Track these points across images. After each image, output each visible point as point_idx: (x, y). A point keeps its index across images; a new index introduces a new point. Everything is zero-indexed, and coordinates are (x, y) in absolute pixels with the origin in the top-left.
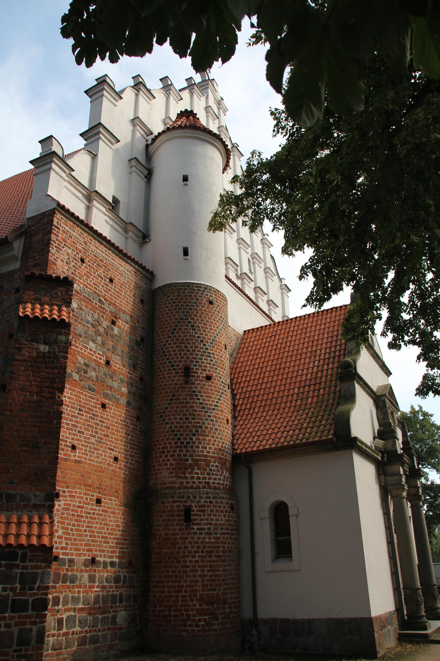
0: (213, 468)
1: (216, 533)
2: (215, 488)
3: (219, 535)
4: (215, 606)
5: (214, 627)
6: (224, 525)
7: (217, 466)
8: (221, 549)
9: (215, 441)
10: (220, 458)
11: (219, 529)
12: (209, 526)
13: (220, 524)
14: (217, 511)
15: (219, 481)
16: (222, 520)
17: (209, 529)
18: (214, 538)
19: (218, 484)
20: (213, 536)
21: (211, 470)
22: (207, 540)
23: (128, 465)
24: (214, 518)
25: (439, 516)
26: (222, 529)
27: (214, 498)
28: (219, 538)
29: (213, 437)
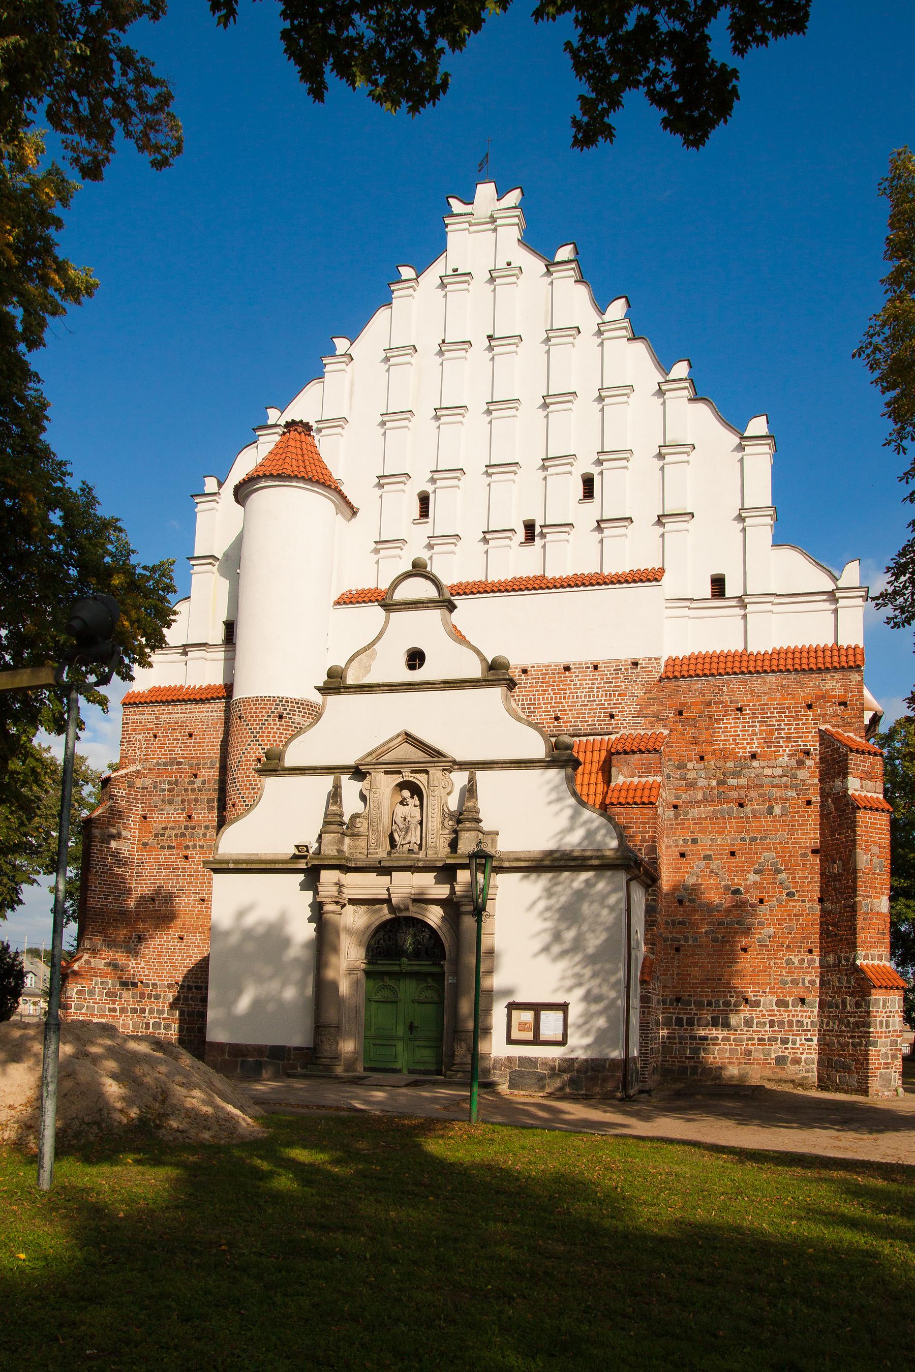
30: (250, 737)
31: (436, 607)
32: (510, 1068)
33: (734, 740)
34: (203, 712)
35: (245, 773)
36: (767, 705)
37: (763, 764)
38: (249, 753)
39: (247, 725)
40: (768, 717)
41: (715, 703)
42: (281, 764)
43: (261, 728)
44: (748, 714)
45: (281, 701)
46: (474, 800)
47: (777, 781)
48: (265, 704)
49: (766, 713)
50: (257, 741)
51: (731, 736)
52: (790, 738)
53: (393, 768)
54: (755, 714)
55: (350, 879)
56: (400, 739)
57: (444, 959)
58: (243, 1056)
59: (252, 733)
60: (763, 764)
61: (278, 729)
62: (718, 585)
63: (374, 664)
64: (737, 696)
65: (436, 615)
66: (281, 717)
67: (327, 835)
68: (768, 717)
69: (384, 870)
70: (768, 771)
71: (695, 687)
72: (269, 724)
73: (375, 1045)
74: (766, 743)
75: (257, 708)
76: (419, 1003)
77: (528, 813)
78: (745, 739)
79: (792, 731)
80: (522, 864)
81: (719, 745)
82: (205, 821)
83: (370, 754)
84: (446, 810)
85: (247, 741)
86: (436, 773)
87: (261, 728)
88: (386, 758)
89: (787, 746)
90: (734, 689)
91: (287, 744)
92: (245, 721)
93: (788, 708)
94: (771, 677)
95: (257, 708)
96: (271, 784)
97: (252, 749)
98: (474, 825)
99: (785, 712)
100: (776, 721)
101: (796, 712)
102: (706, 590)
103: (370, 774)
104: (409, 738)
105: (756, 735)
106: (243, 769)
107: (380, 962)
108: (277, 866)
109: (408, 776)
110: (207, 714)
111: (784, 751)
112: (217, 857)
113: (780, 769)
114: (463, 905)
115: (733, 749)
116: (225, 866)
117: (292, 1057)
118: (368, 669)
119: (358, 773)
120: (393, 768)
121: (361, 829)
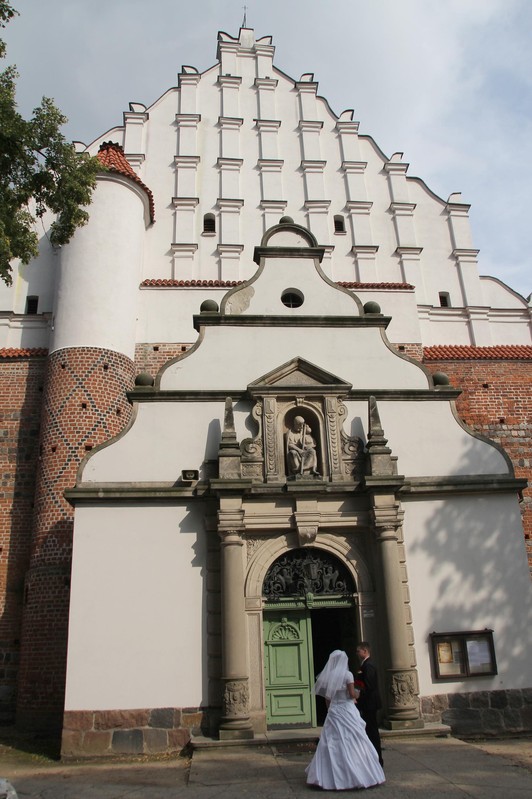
0: (49, 544)
1: (42, 611)
2: (50, 564)
3: (45, 613)
4: (37, 685)
5: (34, 706)
6: (52, 602)
7: (54, 541)
8: (47, 627)
9: (54, 515)
10: (59, 532)
11: (46, 606)
12: (36, 605)
13: (47, 602)
14: (45, 588)
15: (55, 556)
16: (49, 597)
17: (36, 607)
18: (41, 616)
19: (55, 559)
20: (40, 614)
21: (47, 546)
22: (35, 619)
23: (16, 552)
24: (42, 596)
25: (531, 548)
26: (49, 606)
27: (43, 575)
28: (46, 616)
29: (52, 511)
30: (75, 383)
31: (309, 257)
32: (441, 708)
33: (486, 408)
34: (8, 369)
35: (70, 417)
36: (505, 383)
37: (510, 427)
38: (74, 398)
39: (73, 372)
40: (507, 392)
41: (467, 380)
42: (155, 388)
43: (86, 376)
44: (493, 389)
45: (106, 353)
46: (378, 424)
47: (522, 440)
48: (91, 355)
49: (506, 389)
50: (83, 387)
51: (483, 405)
52: (526, 408)
53: (285, 394)
54: (497, 389)
55: (251, 508)
56: (293, 366)
57: (355, 591)
58: (117, 726)
59: (78, 380)
60: (510, 427)
61: (103, 378)
62: (444, 299)
63: (252, 300)
64: (482, 376)
65: (309, 263)
66: (106, 367)
67: (225, 459)
68: (507, 392)
69: (286, 497)
70: (515, 433)
71: (450, 368)
72: (96, 373)
73: (276, 696)
74: (509, 411)
75: (83, 358)
76: (273, 645)
77: (427, 441)
78: (493, 408)
79: (527, 403)
80: (428, 489)
81: (475, 412)
82: (5, 470)
83: (263, 379)
84: (345, 437)
85: (72, 387)
86: (332, 401)
87: (86, 376)
88: (277, 384)
89: (525, 414)
90: (479, 371)
91: (162, 369)
92: (70, 369)
93: (521, 386)
94: (504, 364)
95: (83, 358)
96: (144, 410)
97: (78, 394)
98: (380, 448)
99: (519, 389)
100: (514, 395)
101: (527, 389)
102: (437, 303)
103: (261, 399)
104: (302, 365)
105: (501, 405)
106: (67, 414)
107: (281, 599)
108: (158, 495)
109: (302, 403)
110: (13, 371)
111: (524, 418)
112: (80, 486)
113: (523, 431)
114: (385, 530)
115: (486, 416)
116: (93, 495)
117: (182, 721)
118: (246, 305)
119: (247, 398)
120: (285, 394)
121: (255, 455)
